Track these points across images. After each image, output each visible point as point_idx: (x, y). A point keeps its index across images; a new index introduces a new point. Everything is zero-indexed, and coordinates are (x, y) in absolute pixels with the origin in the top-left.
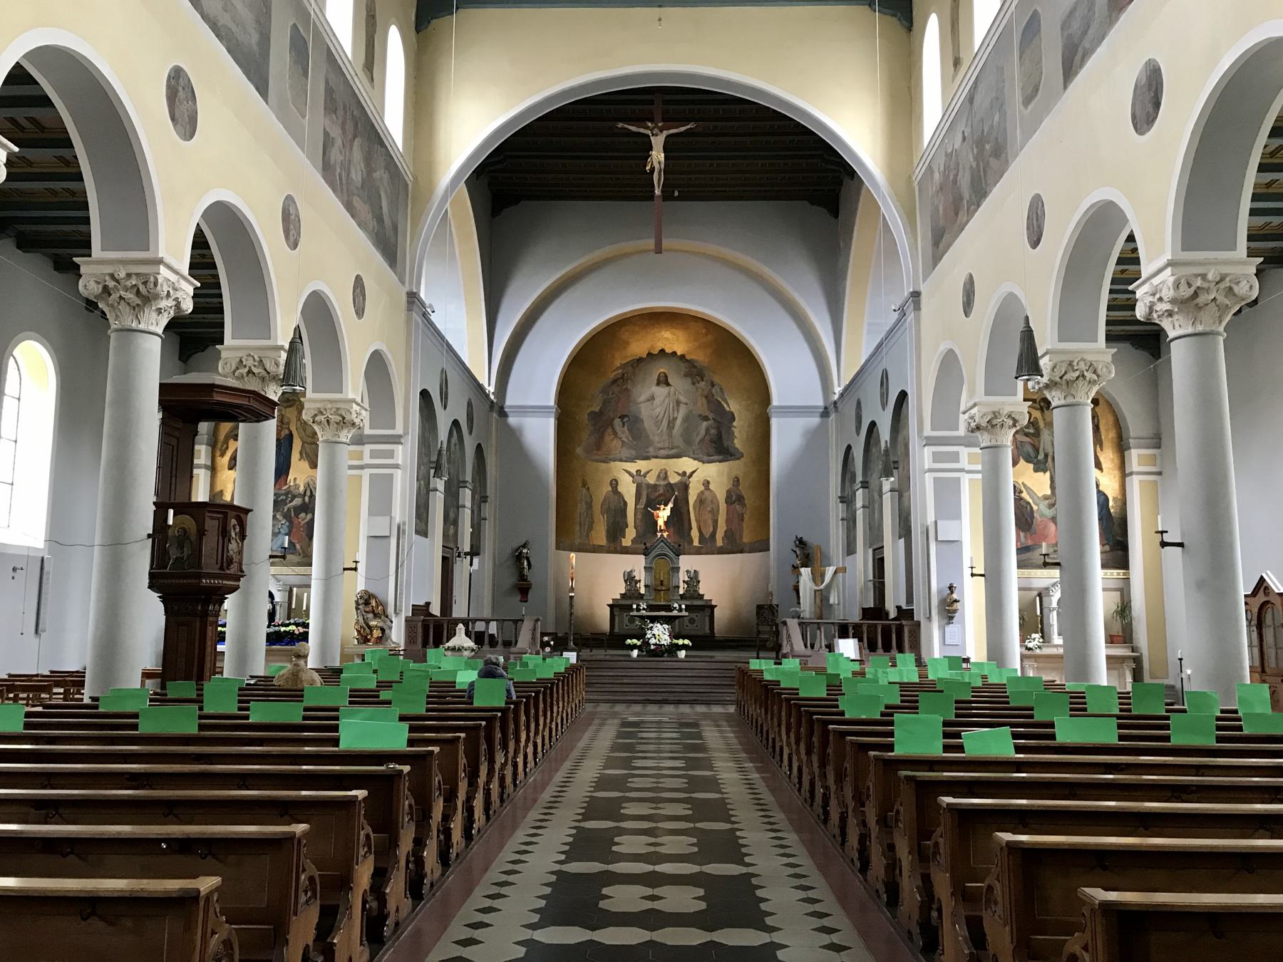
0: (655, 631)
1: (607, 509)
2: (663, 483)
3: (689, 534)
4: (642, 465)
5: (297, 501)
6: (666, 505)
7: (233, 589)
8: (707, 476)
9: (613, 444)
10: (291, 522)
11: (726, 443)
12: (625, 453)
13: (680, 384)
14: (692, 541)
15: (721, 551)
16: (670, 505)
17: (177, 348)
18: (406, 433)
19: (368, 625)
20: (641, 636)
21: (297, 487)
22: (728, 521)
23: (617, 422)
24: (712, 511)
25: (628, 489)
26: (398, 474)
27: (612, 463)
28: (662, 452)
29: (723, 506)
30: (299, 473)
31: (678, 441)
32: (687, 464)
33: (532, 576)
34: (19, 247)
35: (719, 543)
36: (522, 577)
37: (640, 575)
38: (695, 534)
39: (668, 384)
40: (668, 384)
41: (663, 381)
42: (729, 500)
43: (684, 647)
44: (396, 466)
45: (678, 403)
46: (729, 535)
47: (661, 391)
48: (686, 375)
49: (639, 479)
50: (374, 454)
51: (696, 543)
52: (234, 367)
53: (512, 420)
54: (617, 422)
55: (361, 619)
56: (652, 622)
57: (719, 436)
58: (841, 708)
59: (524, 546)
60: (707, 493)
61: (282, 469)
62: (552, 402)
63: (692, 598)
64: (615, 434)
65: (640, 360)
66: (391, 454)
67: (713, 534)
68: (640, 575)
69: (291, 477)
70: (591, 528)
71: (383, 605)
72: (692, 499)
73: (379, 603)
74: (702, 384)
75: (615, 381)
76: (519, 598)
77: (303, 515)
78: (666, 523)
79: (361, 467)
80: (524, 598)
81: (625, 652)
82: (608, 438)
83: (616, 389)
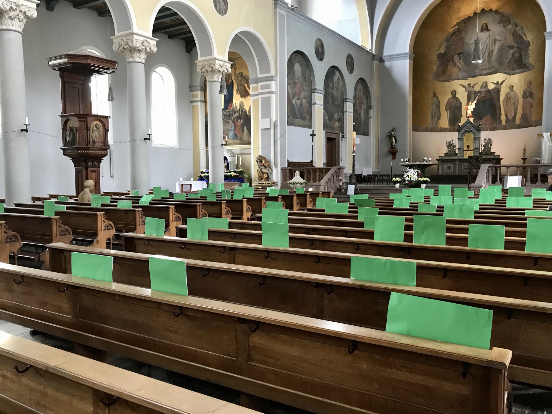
0: (409, 174)
1: (449, 107)
2: (484, 90)
3: (500, 118)
4: (471, 81)
5: (237, 114)
6: (472, 102)
7: (105, 155)
8: (509, 83)
9: (453, 70)
10: (235, 124)
11: (524, 61)
12: (461, 75)
13: (496, 29)
14: (501, 122)
15: (519, 127)
16: (475, 102)
17: (185, 46)
18: (276, 75)
19: (262, 172)
20: (402, 176)
21: (236, 107)
22: (523, 109)
23: (456, 58)
24: (514, 103)
25: (462, 95)
26: (273, 96)
27: (452, 81)
28: (485, 72)
29: (521, 100)
30: (237, 100)
31: (495, 64)
32: (499, 77)
33: (398, 146)
34: (74, 7)
35: (518, 122)
36: (393, 147)
37: (456, 143)
38: (503, 118)
39: (488, 30)
40: (488, 30)
41: (485, 28)
42: (525, 96)
43: (424, 182)
44: (271, 92)
45: (495, 41)
46: (524, 117)
47: (483, 36)
48: (499, 23)
49: (469, 89)
50: (263, 87)
51: (504, 123)
52: (118, 46)
53: (387, 64)
54: (456, 58)
55: (259, 169)
56: (410, 168)
57: (520, 57)
58: (359, 220)
59: (393, 131)
60: (511, 93)
61: (228, 100)
62: (407, 51)
63: (486, 154)
64: (455, 64)
65: (469, 18)
66: (269, 86)
67: (515, 117)
68: (456, 143)
69: (234, 103)
70: (439, 119)
71: (269, 163)
72: (502, 97)
73: (267, 161)
74: (510, 26)
75: (454, 33)
76: (391, 157)
77: (239, 120)
78: (472, 113)
79: (257, 95)
80: (394, 158)
81: (391, 185)
82: (450, 68)
83: (454, 37)
